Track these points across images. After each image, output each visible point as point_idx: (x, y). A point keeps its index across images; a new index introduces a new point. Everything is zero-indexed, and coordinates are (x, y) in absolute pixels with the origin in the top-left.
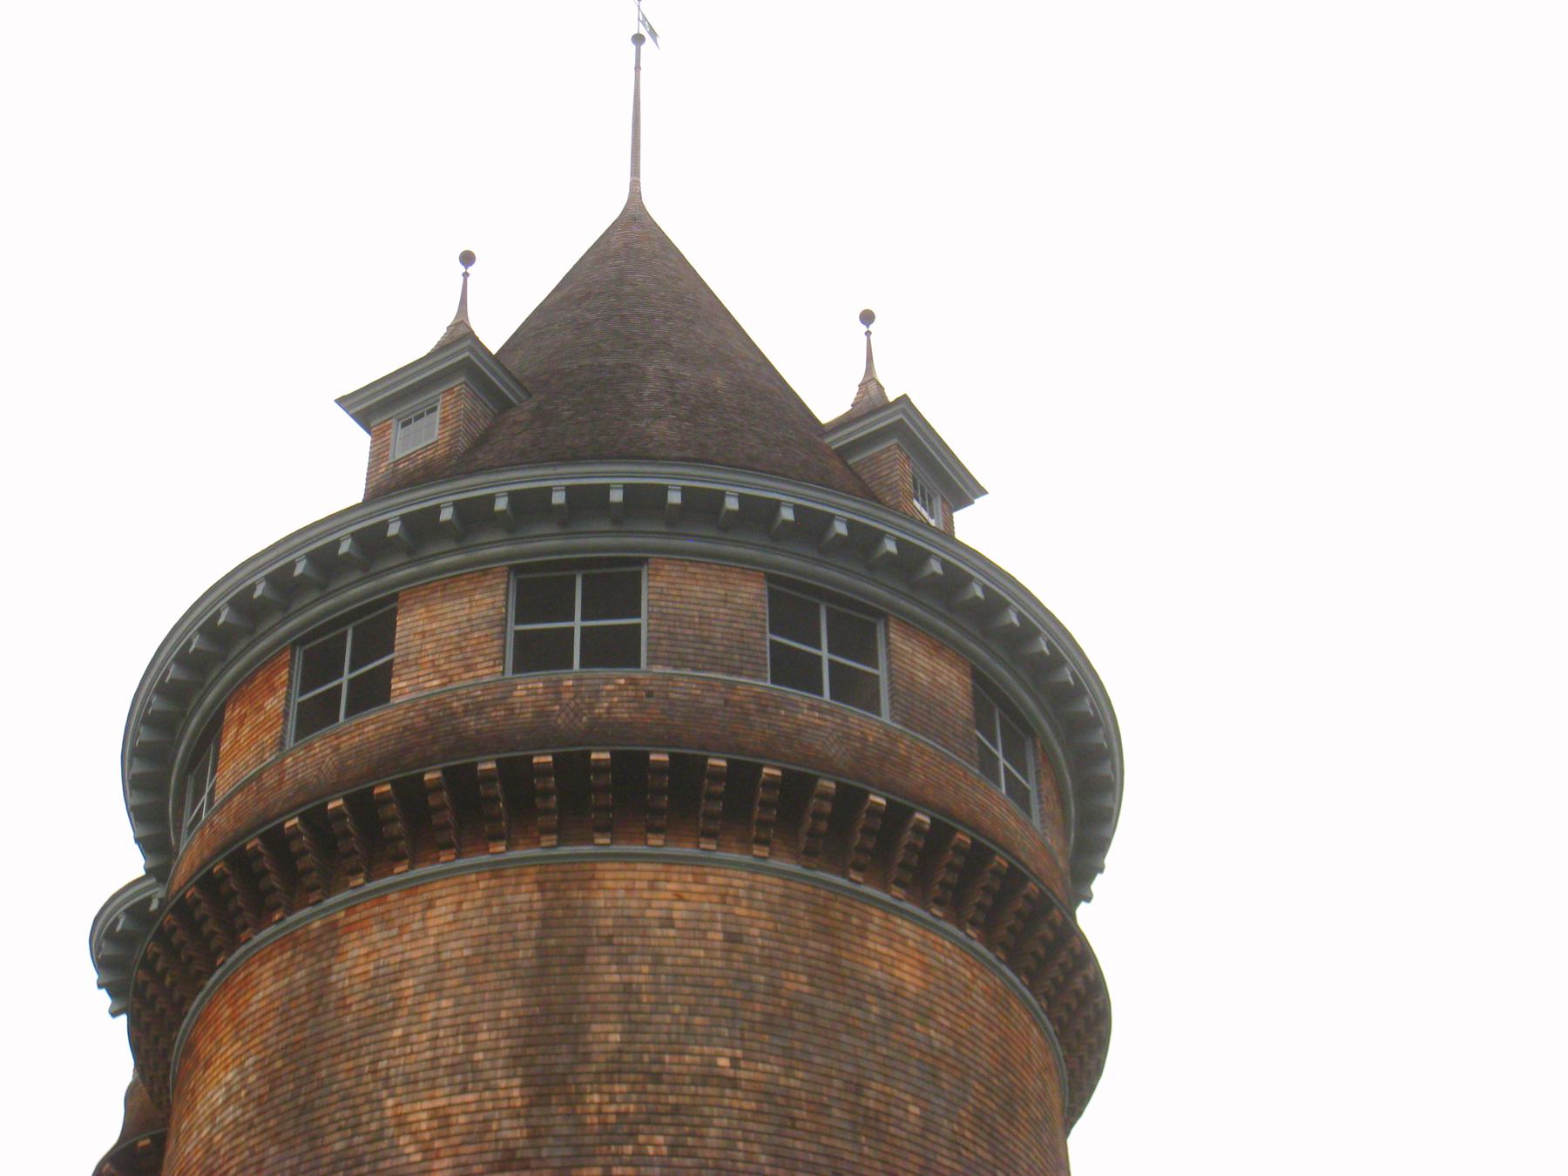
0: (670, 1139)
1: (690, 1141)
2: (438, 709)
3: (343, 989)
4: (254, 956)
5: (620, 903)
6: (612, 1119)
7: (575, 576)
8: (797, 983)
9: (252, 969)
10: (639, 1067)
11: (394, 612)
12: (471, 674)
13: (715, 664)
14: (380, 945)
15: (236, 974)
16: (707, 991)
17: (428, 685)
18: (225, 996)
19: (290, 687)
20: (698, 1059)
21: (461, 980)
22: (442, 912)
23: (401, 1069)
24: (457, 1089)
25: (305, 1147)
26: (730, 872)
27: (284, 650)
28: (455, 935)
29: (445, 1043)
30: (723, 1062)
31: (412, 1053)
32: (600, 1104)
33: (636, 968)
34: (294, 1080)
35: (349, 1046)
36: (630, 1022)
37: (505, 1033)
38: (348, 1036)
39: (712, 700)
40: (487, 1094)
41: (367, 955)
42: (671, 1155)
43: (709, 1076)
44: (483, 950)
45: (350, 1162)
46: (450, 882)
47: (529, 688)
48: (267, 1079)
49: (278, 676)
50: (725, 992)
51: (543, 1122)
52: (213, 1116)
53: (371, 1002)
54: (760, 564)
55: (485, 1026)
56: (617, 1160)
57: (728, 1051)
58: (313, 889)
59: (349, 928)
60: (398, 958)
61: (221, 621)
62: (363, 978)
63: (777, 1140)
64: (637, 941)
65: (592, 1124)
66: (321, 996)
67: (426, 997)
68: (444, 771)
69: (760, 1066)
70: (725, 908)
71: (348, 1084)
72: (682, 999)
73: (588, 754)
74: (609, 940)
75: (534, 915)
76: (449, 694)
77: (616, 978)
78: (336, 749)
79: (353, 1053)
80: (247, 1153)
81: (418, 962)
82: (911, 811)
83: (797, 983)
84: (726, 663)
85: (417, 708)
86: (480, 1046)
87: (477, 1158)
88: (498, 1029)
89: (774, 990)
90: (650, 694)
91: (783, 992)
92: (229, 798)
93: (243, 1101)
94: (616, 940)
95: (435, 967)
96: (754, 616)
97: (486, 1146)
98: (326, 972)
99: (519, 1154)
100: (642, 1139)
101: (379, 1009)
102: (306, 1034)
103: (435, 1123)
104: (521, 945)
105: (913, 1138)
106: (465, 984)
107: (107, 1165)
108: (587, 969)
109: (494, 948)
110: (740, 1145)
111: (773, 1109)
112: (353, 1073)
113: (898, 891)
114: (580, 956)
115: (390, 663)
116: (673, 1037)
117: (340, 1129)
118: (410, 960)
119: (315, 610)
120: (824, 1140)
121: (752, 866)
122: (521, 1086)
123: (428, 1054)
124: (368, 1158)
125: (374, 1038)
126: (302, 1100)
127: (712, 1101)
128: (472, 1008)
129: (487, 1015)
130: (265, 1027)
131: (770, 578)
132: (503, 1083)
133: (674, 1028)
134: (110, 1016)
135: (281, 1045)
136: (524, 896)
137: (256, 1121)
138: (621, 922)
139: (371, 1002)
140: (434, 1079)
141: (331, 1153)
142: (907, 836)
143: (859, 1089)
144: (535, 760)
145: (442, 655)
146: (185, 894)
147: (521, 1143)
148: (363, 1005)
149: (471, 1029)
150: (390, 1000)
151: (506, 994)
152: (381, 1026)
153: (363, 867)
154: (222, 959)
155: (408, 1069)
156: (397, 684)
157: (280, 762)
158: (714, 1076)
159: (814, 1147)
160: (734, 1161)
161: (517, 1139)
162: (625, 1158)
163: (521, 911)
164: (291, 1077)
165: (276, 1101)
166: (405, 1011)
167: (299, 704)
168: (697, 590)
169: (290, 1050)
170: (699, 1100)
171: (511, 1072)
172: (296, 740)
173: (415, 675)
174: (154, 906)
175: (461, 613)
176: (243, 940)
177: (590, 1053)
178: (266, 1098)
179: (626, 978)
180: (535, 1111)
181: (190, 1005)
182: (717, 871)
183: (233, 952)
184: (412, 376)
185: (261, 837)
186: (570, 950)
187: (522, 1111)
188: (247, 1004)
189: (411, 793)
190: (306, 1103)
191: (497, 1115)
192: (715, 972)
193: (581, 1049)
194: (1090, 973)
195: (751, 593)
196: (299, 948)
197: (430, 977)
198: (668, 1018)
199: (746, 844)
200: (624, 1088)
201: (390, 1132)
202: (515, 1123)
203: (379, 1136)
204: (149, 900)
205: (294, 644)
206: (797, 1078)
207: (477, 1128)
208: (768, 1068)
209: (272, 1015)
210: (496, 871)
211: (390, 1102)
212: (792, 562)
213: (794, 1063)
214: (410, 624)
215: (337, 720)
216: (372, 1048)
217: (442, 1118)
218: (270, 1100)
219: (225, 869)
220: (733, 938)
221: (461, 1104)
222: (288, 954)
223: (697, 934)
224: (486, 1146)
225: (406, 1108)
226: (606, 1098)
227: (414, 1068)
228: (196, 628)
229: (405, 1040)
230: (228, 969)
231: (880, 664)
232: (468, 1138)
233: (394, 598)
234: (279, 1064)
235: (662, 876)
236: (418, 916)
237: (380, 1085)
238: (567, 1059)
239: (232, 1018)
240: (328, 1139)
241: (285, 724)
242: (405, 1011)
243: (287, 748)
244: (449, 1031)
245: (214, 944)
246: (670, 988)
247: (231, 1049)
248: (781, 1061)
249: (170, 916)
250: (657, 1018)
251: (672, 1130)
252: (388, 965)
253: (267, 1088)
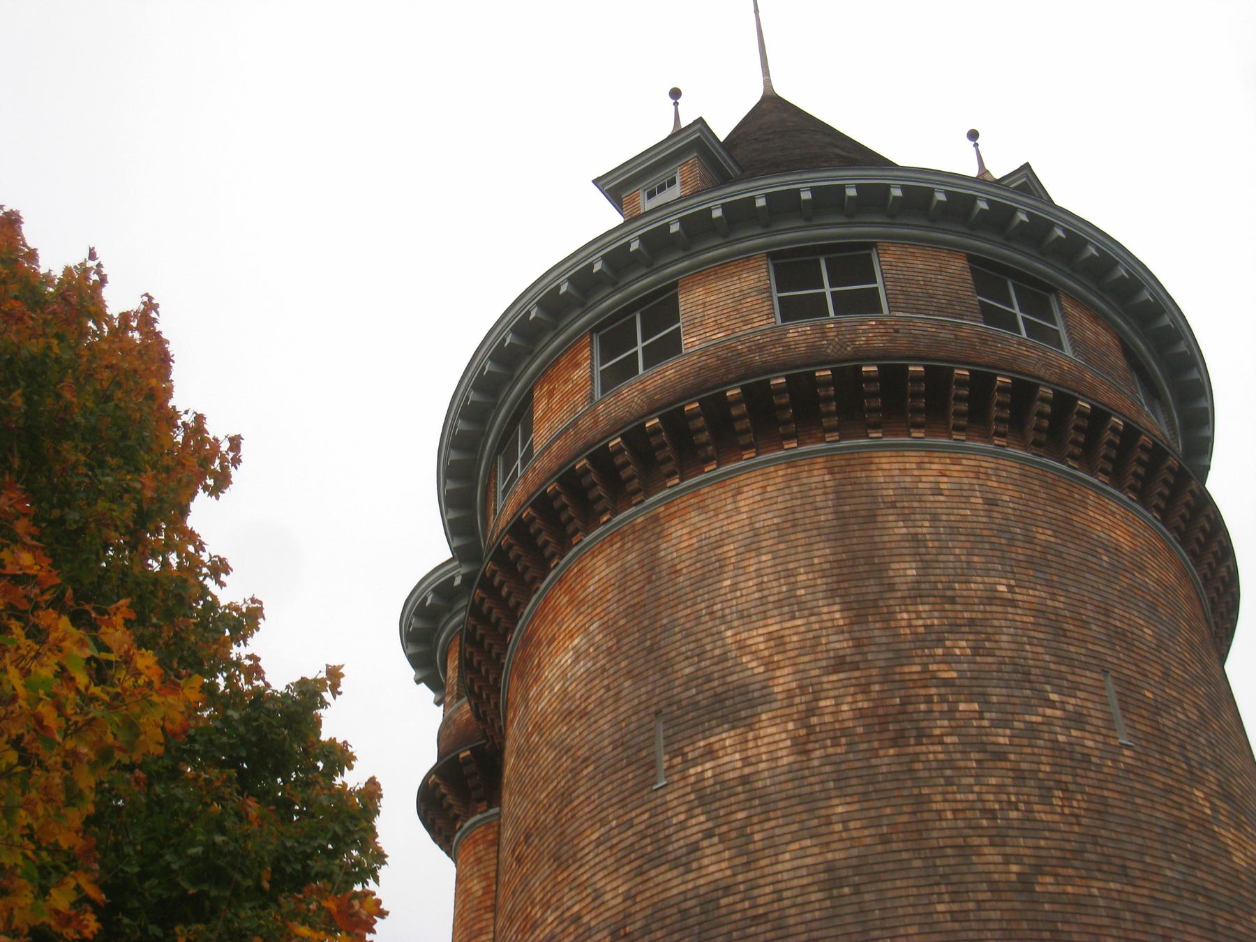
0: (971, 644)
1: (987, 644)
3: (673, 559)
5: (896, 479)
6: (922, 630)
7: (819, 260)
8: (1044, 535)
9: (584, 563)
10: (936, 593)
11: (676, 296)
12: (750, 326)
13: (940, 311)
14: (699, 525)
15: (570, 570)
16: (978, 539)
17: (714, 337)
19: (592, 359)
20: (981, 586)
21: (775, 541)
22: (749, 497)
23: (734, 609)
24: (787, 617)
25: (658, 676)
26: (978, 457)
28: (764, 510)
29: (770, 585)
30: (1002, 588)
31: (742, 596)
32: (909, 620)
33: (919, 523)
34: (638, 630)
36: (922, 561)
37: (820, 574)
39: (944, 335)
40: (813, 619)
41: (690, 533)
42: (974, 655)
43: (991, 598)
44: (790, 517)
45: (700, 681)
46: (753, 474)
47: (799, 333)
48: (612, 635)
50: (993, 539)
51: (864, 634)
52: (564, 673)
53: (698, 565)
54: (965, 247)
55: (802, 570)
56: (931, 660)
57: (1004, 581)
59: (671, 516)
60: (718, 531)
62: (688, 550)
63: (1054, 644)
64: (916, 505)
65: (905, 634)
66: (653, 568)
67: (748, 555)
68: (742, 387)
69: (1031, 592)
70: (980, 482)
71: (688, 625)
72: (959, 544)
73: (860, 367)
74: (893, 505)
75: (828, 490)
77: (904, 531)
78: (643, 390)
79: (689, 603)
80: (602, 691)
81: (736, 532)
82: (1110, 415)
83: (1044, 535)
84: (950, 311)
86: (799, 585)
87: (813, 665)
88: (813, 572)
89: (1030, 540)
90: (897, 331)
91: (1037, 541)
92: (549, 447)
94: (898, 505)
95: (751, 534)
96: (964, 280)
97: (820, 656)
99: (848, 659)
100: (948, 643)
101: (706, 569)
102: (645, 596)
103: (772, 643)
104: (822, 511)
105: (1152, 651)
106: (780, 543)
107: (433, 777)
108: (879, 525)
109: (798, 516)
110: (1028, 648)
111: (1047, 622)
112: (692, 617)
113: (1102, 477)
114: (872, 517)
115: (679, 328)
116: (959, 571)
117: (687, 658)
118: (729, 531)
119: (609, 302)
120: (1090, 646)
121: (993, 452)
122: (841, 611)
123: (756, 595)
124: (716, 675)
125: (706, 589)
127: (999, 616)
128: (789, 559)
129: (802, 563)
130: (604, 600)
131: (972, 259)
132: (825, 610)
133: (958, 564)
135: (621, 609)
136: (817, 476)
137: (608, 666)
138: (899, 492)
139: (698, 565)
140: (765, 612)
141: (682, 676)
142: (1108, 435)
143: (1107, 612)
144: (817, 374)
147: (848, 651)
149: (791, 573)
151: (816, 547)
152: (711, 581)
155: (740, 608)
156: (685, 340)
157: (593, 410)
158: (996, 598)
159: (1083, 651)
160: (1025, 659)
161: (844, 648)
162: (938, 659)
163: (816, 488)
164: (636, 629)
165: (624, 649)
166: (731, 567)
168: (919, 264)
170: (988, 616)
171: (831, 601)
174: (458, 581)
175: (733, 287)
177: (894, 584)
178: (614, 648)
179: (912, 530)
180: (856, 628)
182: (968, 456)
183: (563, 557)
184: (656, 155)
185: (587, 457)
186: (863, 513)
187: (845, 628)
188: (585, 588)
189: (716, 407)
190: (652, 645)
191: (824, 632)
192: (982, 526)
193: (887, 581)
194: (1230, 563)
195: (958, 266)
197: (748, 541)
198: (951, 558)
199: (987, 438)
200: (927, 607)
201: (733, 654)
202: (841, 637)
203: (723, 658)
204: (452, 579)
205: (592, 331)
206: (1060, 602)
207: (808, 643)
208: (1037, 593)
209: (610, 589)
210: (791, 462)
211: (729, 633)
212: (985, 245)
213: (1056, 591)
214: (690, 302)
216: (706, 596)
217: (778, 641)
218: (619, 649)
220: (991, 503)
221: (793, 627)
222: (618, 545)
223: (963, 500)
224: (820, 656)
225: (744, 636)
226: (913, 616)
227: (746, 606)
229: (734, 587)
230: (561, 570)
231: (1058, 322)
232: (802, 651)
233: (675, 285)
234: (622, 622)
235: (926, 460)
236: (729, 501)
237: (717, 622)
238: (876, 589)
239: (570, 602)
242: (731, 567)
243: (596, 399)
244: (772, 577)
245: (547, 552)
246: (948, 537)
247: (571, 623)
248: (1045, 588)
249: (507, 536)
250: (942, 558)
251: (971, 637)
252: (710, 537)
253: (615, 641)
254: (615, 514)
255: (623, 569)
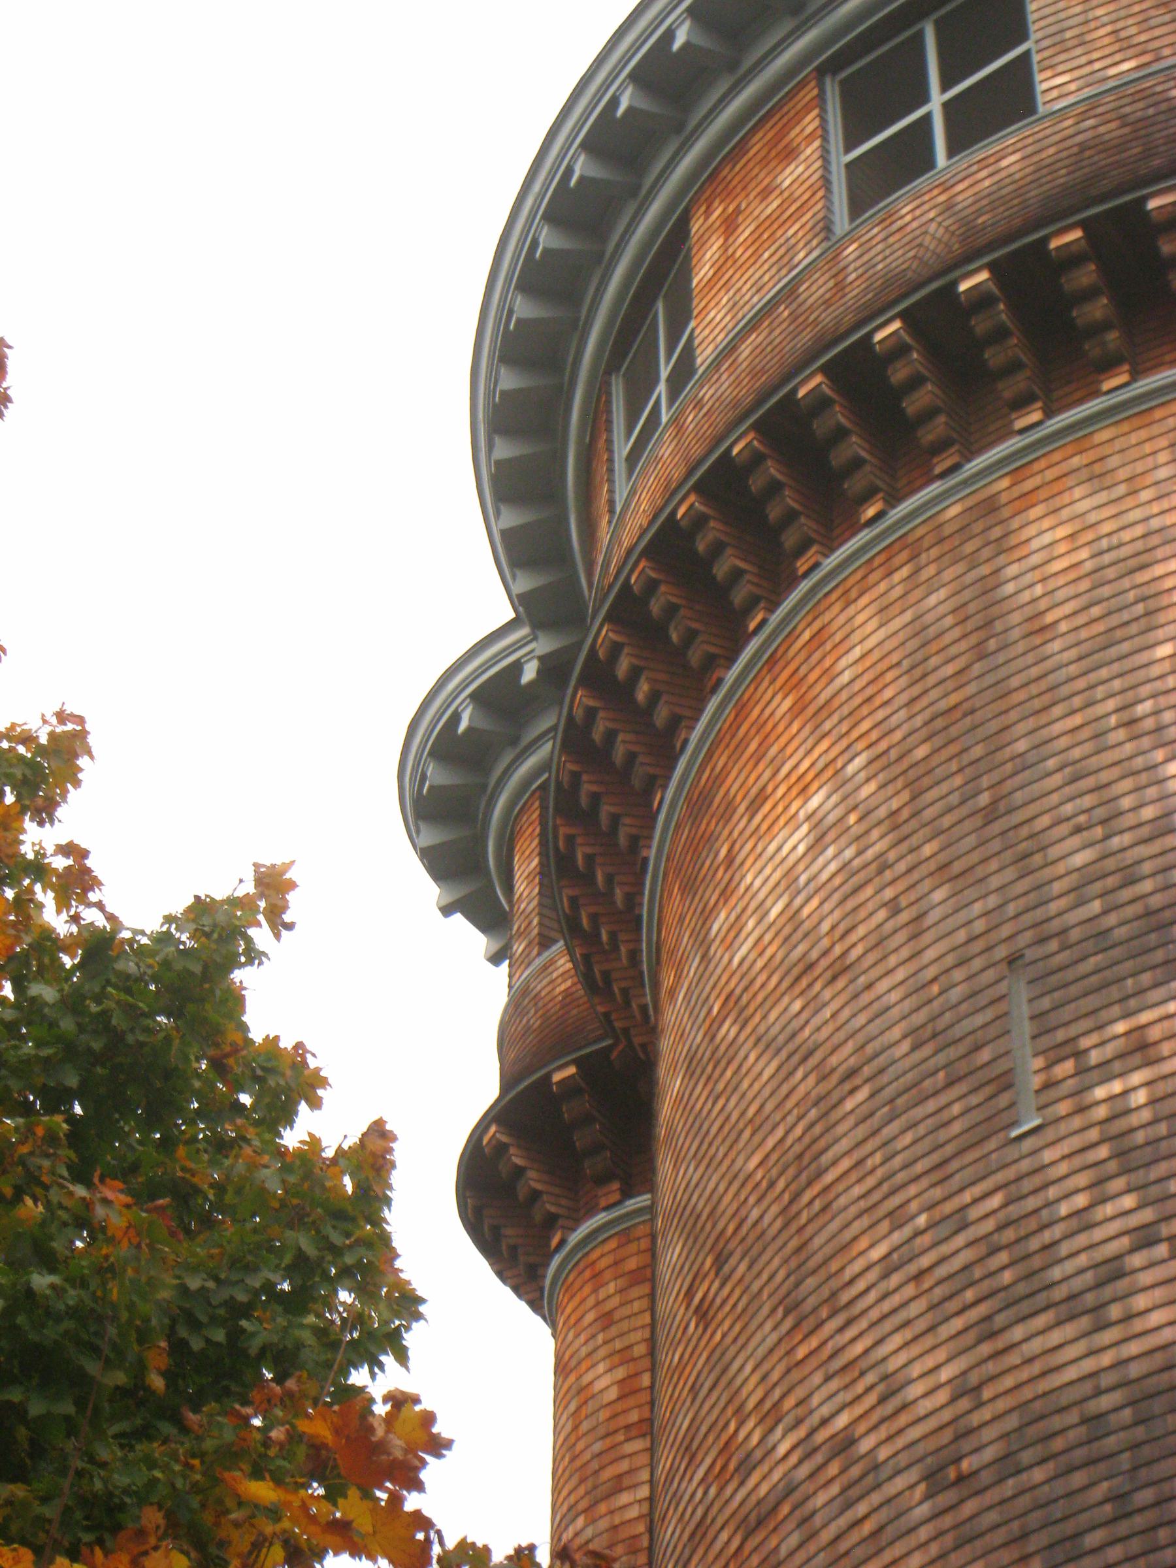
2: (1141, 105)
4: (827, 595)
14: (1093, 518)
15: (792, 636)
17: (1113, 71)
18: (772, 682)
19: (825, 138)
25: (1010, 874)
27: (802, 85)
35: (1065, 690)
38: (1062, 674)
41: (1072, 536)
49: (797, 129)
53: (1096, 611)
58: (940, 447)
59: (1026, 500)
60: (1138, 530)
61: (677, 45)
62: (1072, 575)
66: (990, 623)
76: (1160, 78)
78: (949, 206)
79: (1077, 701)
85: (1099, 110)
92: (731, 348)
93: (856, 830)
98: (990, 585)
101: (1115, 620)
107: (493, 1129)
112: (1085, 733)
115: (1027, 55)
117: (1078, 830)
125: (1116, 668)
126: (984, 799)
130: (877, 701)
134: (317, 1112)
135: (918, 721)
137: (892, 856)
139: (1096, 611)
145: (1130, 21)
146: (674, 512)
148: (1081, 619)
150: (1136, 602)
152: (1125, 647)
153: (1037, 391)
154: (759, 617)
157: (832, 256)
167: (848, 166)
169: (939, 723)
172: (853, 218)
173: (1083, 60)
174: (529, 673)
176: (801, 572)
181: (692, 728)
183: (777, 604)
185: (824, 369)
188: (830, 675)
196: (924, 556)
209: (889, 676)
215: (930, 164)
219: (755, 443)
228: (538, 217)
234: (921, 752)
239: (797, 710)
240: (1054, 852)
241: (827, 197)
249: (692, 498)
252: (1120, 545)
254: (894, 499)
255: (918, 628)
